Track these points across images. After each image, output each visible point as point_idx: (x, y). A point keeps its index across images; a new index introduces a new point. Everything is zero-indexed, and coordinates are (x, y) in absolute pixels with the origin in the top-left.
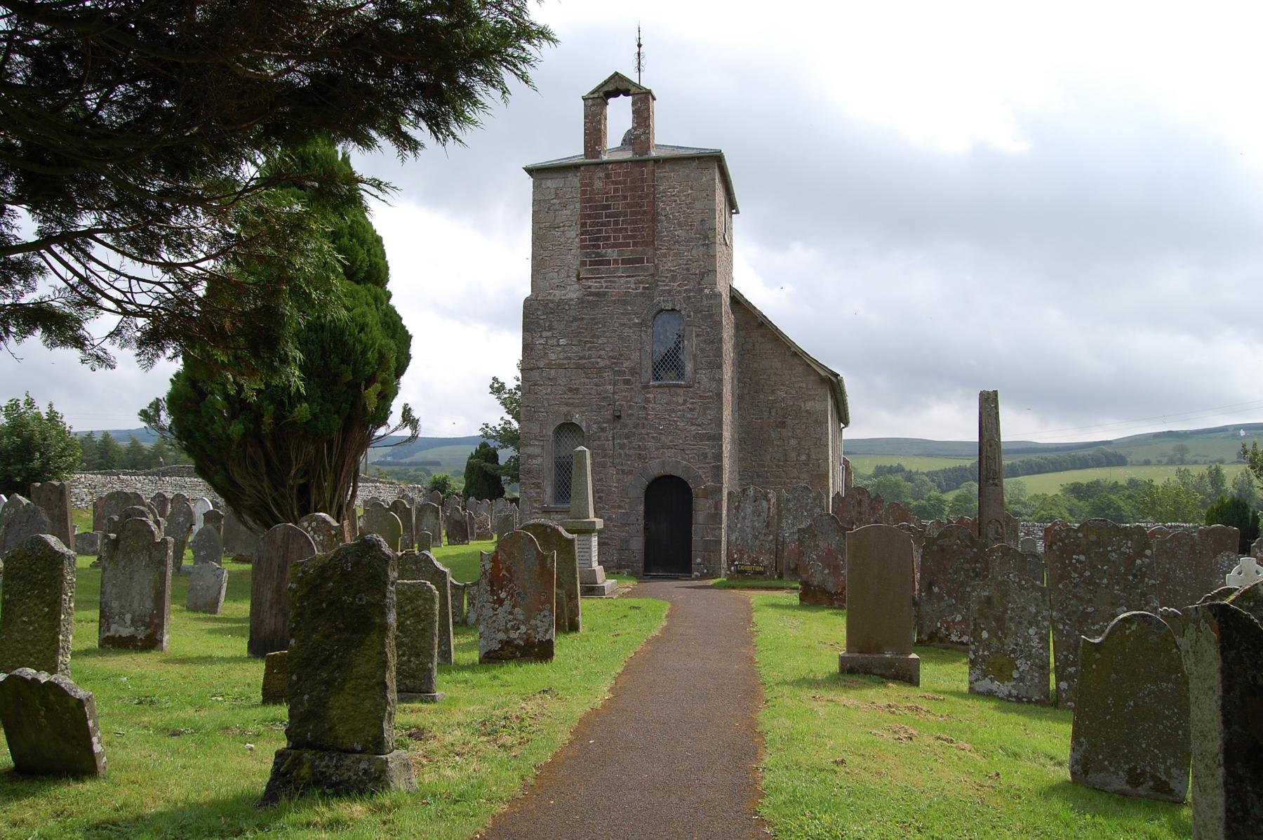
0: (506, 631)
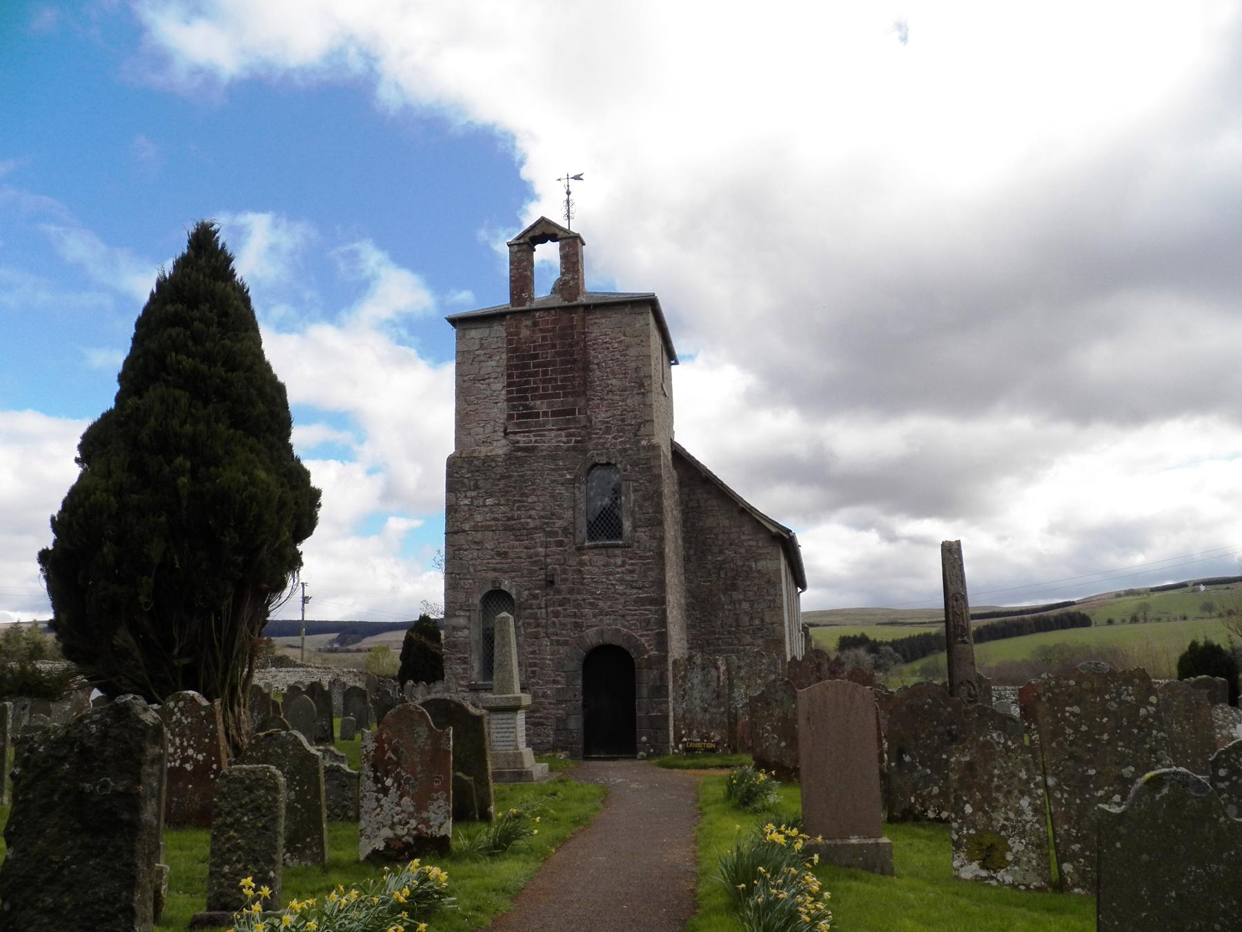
0: (392, 827)
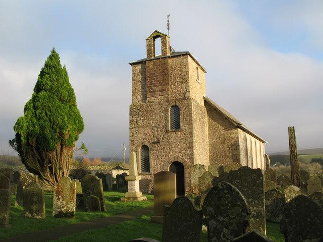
0: (60, 208)
